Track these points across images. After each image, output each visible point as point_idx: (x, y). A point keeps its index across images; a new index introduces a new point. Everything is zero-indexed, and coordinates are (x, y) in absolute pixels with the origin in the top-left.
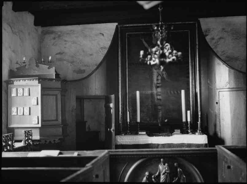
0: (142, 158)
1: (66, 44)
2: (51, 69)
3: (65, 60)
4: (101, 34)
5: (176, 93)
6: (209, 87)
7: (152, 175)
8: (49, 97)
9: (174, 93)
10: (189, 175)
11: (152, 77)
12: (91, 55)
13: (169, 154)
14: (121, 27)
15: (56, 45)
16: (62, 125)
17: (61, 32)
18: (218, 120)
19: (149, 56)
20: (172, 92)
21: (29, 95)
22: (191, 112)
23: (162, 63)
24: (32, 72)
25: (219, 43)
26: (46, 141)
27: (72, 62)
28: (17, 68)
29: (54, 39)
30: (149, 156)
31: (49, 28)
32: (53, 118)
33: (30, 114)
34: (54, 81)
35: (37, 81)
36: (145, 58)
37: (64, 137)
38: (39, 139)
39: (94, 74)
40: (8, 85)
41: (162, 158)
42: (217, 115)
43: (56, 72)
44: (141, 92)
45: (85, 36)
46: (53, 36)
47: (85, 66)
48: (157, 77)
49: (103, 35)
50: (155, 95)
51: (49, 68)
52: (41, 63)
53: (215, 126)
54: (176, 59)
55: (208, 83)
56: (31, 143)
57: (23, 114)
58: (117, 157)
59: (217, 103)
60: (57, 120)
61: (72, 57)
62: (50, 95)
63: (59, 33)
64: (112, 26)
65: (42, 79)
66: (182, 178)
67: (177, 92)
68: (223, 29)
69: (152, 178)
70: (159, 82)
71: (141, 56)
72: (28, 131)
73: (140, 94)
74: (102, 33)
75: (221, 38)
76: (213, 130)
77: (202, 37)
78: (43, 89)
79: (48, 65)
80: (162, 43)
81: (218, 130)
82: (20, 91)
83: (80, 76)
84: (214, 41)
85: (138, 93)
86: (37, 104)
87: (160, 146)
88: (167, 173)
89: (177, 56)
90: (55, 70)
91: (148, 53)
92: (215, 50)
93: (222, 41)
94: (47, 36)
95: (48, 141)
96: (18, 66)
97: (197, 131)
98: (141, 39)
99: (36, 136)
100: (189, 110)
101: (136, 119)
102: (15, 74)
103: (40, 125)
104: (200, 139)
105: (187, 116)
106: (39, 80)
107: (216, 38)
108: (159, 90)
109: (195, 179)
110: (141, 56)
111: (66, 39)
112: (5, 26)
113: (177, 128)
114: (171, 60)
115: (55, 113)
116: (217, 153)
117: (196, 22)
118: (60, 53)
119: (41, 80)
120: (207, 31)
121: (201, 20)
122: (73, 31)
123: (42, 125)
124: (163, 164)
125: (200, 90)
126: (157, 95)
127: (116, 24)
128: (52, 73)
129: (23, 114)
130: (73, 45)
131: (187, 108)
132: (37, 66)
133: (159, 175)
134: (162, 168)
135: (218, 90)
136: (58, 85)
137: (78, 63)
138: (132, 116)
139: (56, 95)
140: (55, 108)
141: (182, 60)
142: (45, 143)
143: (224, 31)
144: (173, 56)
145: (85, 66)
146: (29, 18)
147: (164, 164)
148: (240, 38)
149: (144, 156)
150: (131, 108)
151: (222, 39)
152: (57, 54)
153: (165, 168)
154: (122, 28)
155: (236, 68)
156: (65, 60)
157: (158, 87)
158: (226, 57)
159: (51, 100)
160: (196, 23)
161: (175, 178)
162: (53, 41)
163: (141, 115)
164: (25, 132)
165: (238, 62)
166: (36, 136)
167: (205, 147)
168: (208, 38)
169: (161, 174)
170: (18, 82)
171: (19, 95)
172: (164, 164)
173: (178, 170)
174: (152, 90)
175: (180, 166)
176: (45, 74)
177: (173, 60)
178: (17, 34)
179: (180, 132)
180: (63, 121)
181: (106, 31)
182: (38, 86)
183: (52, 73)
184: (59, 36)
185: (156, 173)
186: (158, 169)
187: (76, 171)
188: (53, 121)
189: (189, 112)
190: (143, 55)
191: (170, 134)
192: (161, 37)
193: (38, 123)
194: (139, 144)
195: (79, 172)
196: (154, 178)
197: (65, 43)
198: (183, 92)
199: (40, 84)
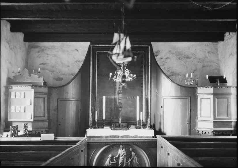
0: (107, 145)
1: (48, 57)
2: (41, 78)
3: (47, 69)
4: (76, 50)
5: (133, 98)
6: (156, 95)
7: (114, 156)
8: (39, 99)
9: (131, 98)
10: (139, 157)
11: (115, 85)
12: (68, 66)
13: (126, 142)
14: (92, 47)
15: (40, 57)
16: (48, 120)
17: (44, 47)
18: (162, 119)
19: (115, 76)
20: (130, 98)
21: (25, 97)
22: (143, 113)
23: (124, 81)
24: (26, 80)
25: (166, 61)
26: (36, 132)
27: (53, 72)
28: (14, 77)
29: (39, 52)
30: (112, 143)
31: (34, 43)
32: (42, 115)
33: (25, 112)
34: (43, 87)
35: (31, 87)
36: (113, 78)
37: (49, 129)
38: (31, 130)
39: (72, 83)
40: (8, 90)
41: (121, 144)
42: (162, 115)
43: (44, 80)
44: (107, 97)
45: (64, 51)
46: (37, 50)
47: (63, 75)
48: (119, 86)
49: (78, 51)
50: (117, 99)
51: (39, 77)
52: (33, 73)
53: (160, 123)
54: (132, 80)
55: (156, 92)
56: (27, 132)
57: (20, 112)
58: (91, 143)
59: (162, 107)
60: (44, 116)
61: (53, 67)
62: (39, 98)
63: (43, 48)
64: (87, 44)
65: (34, 86)
66: (135, 159)
67: (134, 98)
68: (170, 51)
69: (113, 159)
70: (120, 90)
71: (110, 76)
72: (26, 124)
73: (107, 99)
74: (77, 49)
75: (167, 58)
76: (159, 127)
77: (153, 57)
78: (35, 93)
79: (38, 75)
80: (124, 69)
81: (162, 127)
82: (18, 94)
83: (58, 83)
84: (163, 60)
85: (104, 98)
86: (31, 104)
87: (120, 137)
88: (125, 155)
89: (133, 78)
90: (163, 138)
91: (114, 74)
92: (161, 67)
93: (168, 60)
94: (32, 49)
95: (37, 132)
96: (13, 75)
97: (147, 127)
98: (108, 57)
99: (30, 128)
100: (142, 112)
101: (102, 117)
102: (11, 82)
103: (32, 120)
104: (148, 133)
105: (140, 116)
106: (32, 86)
107: (164, 58)
108: (120, 96)
109: (145, 164)
110: (110, 76)
111: (48, 52)
112: (3, 43)
113: (133, 125)
114: (129, 80)
115: (43, 112)
116: (157, 142)
117: (150, 46)
118: (43, 64)
119: (33, 87)
120: (157, 52)
121: (153, 44)
122: (53, 47)
123: (34, 120)
124: (121, 149)
125: (151, 97)
126: (119, 99)
127: (88, 43)
128: (41, 81)
129: (20, 112)
130: (53, 58)
131: (141, 110)
132: (30, 76)
133: (119, 157)
134: (121, 152)
135: (163, 98)
136: (45, 90)
137: (58, 72)
138: (99, 114)
139: (44, 98)
140: (43, 108)
141: (136, 80)
142: (36, 133)
143: (170, 53)
144: (130, 78)
145: (63, 75)
146: (20, 36)
147: (123, 149)
148: (182, 58)
149: (108, 143)
150: (99, 109)
151: (168, 59)
152: (41, 64)
153: (123, 152)
154: (94, 48)
155: (177, 82)
156: (47, 69)
157: (119, 93)
158: (171, 72)
159: (41, 102)
160: (149, 47)
161: (130, 159)
162: (37, 54)
163: (106, 114)
164: (24, 124)
165: (179, 76)
166: (30, 128)
167: (152, 138)
168: (157, 58)
169: (120, 156)
170: (15, 88)
171: (16, 97)
172: (123, 149)
173: (132, 153)
174: (115, 96)
175: (133, 150)
176: (36, 81)
177: (131, 80)
178: (13, 49)
179: (134, 127)
180: (49, 117)
181: (80, 48)
182: (32, 91)
183: (41, 81)
184: (43, 50)
185: (117, 155)
186: (118, 152)
187: (73, 146)
188: (41, 117)
189: (141, 113)
190: (111, 76)
191: (128, 129)
192: (123, 65)
193: (31, 118)
194: (71, 166)
195: (73, 147)
196: (115, 159)
197: (47, 56)
198: (138, 98)
199: (33, 90)
